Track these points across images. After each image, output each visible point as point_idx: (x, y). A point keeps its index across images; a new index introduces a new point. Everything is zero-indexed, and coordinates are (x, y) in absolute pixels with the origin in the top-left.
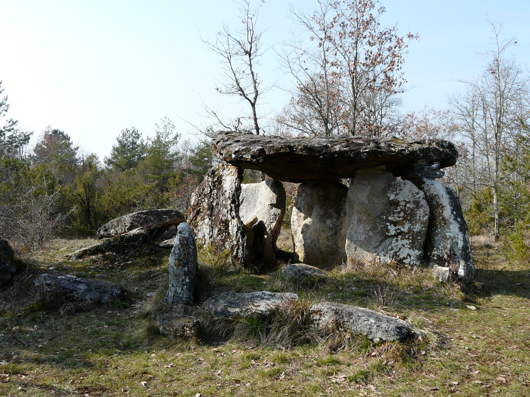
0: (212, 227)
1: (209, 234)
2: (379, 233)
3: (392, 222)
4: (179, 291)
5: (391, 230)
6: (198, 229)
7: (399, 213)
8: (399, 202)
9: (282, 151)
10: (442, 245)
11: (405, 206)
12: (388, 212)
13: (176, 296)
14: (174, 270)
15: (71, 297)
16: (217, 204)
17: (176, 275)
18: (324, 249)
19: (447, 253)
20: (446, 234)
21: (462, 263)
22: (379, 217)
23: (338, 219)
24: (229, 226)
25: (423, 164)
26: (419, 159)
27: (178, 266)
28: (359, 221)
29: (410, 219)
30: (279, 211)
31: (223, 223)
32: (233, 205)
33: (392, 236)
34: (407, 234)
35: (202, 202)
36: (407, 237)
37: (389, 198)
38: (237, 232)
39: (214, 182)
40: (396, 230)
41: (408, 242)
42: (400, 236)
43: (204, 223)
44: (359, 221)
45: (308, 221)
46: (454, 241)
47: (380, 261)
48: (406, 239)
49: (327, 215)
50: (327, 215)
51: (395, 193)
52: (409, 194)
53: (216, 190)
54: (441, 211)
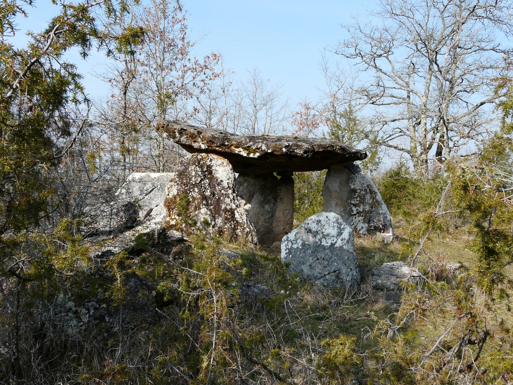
0: (213, 216)
7: (357, 198)
9: (329, 149)
10: (376, 219)
11: (360, 193)
14: (354, 256)
16: (213, 194)
23: (274, 204)
24: (235, 215)
28: (337, 205)
32: (235, 195)
34: (362, 212)
35: (191, 192)
36: (362, 215)
49: (266, 201)
50: (266, 201)
53: (207, 180)
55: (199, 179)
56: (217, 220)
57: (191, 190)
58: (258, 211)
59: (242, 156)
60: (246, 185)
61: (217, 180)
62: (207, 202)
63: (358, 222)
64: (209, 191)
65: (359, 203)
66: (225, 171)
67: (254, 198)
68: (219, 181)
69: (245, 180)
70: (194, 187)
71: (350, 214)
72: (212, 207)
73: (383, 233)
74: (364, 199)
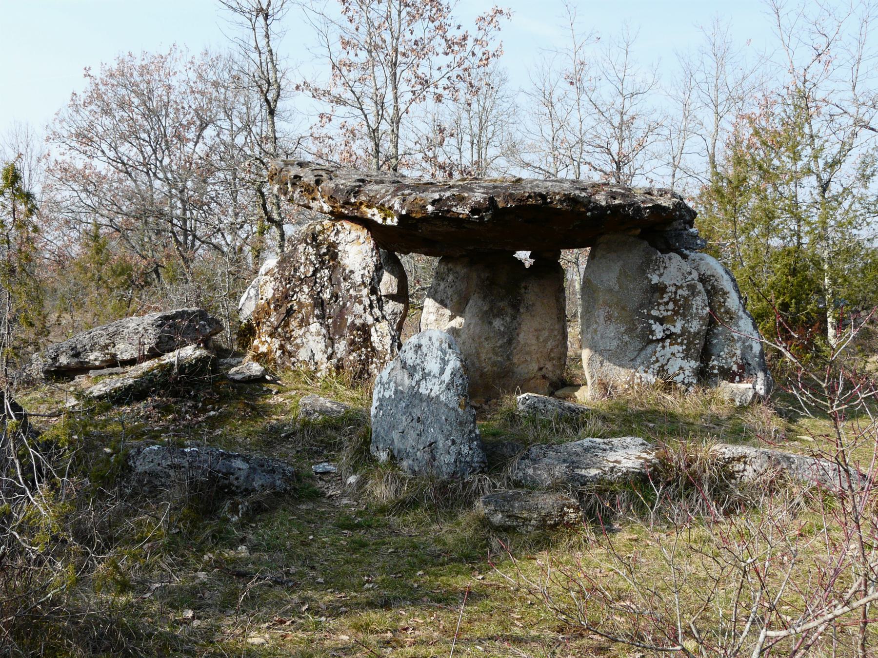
0: (330, 338)
1: (325, 352)
2: (637, 336)
3: (657, 319)
4: (466, 451)
5: (657, 331)
6: (297, 345)
7: (667, 303)
8: (666, 287)
9: (531, 201)
10: (726, 350)
11: (676, 293)
12: (650, 303)
13: (461, 462)
14: (458, 414)
15: (226, 486)
16: (335, 296)
17: (461, 424)
18: (487, 369)
19: (736, 363)
20: (733, 334)
21: (761, 375)
22: (636, 311)
23: (514, 318)
24: (370, 336)
25: (680, 227)
26: (675, 220)
27: (466, 406)
28: (609, 318)
29: (684, 313)
30: (401, 306)
31: (358, 330)
32: (374, 297)
33: (658, 341)
34: (679, 336)
35: (295, 292)
36: (679, 340)
37: (651, 280)
38: (392, 345)
39: (320, 256)
40: (664, 331)
41: (680, 349)
42: (668, 341)
43: (308, 331)
44: (609, 318)
45: (458, 322)
46: (747, 344)
47: (641, 381)
48: (678, 344)
49: (495, 311)
50: (495, 311)
51: (657, 272)
52: (678, 274)
53: (326, 271)
54: (722, 300)
55: (312, 269)
56: (336, 345)
57: (297, 290)
58: (477, 331)
59: (376, 222)
60: (450, 278)
61: (344, 270)
62: (323, 310)
63: (669, 356)
64: (328, 290)
65: (673, 315)
66: (360, 252)
67: (469, 305)
68: (347, 271)
69: (449, 270)
70: (301, 284)
71: (648, 340)
72: (330, 321)
73: (738, 382)
74: (687, 306)
